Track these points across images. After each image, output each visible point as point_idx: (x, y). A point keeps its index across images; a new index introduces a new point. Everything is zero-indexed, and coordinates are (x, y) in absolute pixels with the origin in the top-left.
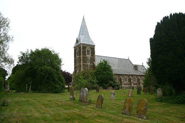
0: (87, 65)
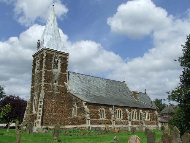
0: (53, 87)
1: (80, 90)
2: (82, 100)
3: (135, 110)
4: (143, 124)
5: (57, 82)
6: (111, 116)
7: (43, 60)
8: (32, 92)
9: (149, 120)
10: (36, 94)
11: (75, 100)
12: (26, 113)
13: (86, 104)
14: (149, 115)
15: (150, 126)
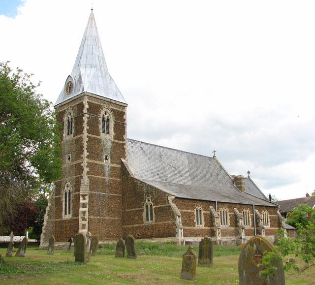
0: (103, 167)
1: (149, 174)
4: (260, 234)
7: (83, 115)
9: (269, 226)
11: (148, 194)
12: (46, 217)
13: (174, 201)
14: (269, 217)
15: (270, 236)
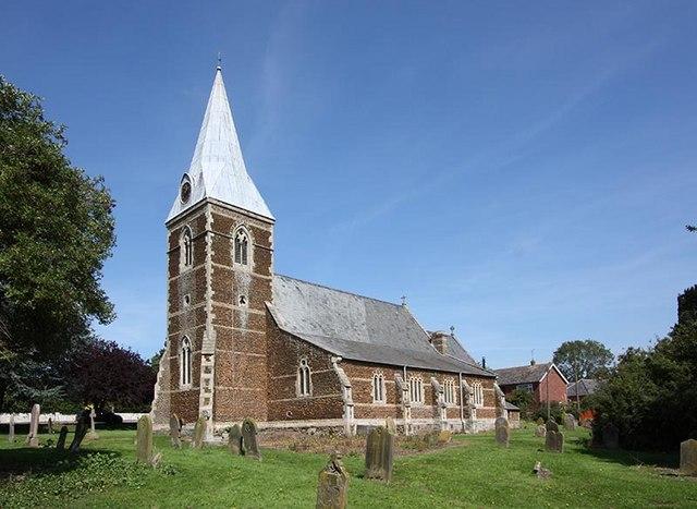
0: (237, 314)
2: (327, 353)
3: (452, 380)
5: (247, 302)
6: (401, 396)
7: (206, 234)
8: (174, 325)
10: (187, 332)
12: (157, 387)
